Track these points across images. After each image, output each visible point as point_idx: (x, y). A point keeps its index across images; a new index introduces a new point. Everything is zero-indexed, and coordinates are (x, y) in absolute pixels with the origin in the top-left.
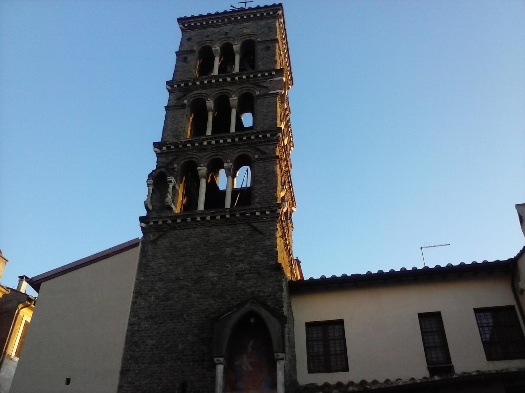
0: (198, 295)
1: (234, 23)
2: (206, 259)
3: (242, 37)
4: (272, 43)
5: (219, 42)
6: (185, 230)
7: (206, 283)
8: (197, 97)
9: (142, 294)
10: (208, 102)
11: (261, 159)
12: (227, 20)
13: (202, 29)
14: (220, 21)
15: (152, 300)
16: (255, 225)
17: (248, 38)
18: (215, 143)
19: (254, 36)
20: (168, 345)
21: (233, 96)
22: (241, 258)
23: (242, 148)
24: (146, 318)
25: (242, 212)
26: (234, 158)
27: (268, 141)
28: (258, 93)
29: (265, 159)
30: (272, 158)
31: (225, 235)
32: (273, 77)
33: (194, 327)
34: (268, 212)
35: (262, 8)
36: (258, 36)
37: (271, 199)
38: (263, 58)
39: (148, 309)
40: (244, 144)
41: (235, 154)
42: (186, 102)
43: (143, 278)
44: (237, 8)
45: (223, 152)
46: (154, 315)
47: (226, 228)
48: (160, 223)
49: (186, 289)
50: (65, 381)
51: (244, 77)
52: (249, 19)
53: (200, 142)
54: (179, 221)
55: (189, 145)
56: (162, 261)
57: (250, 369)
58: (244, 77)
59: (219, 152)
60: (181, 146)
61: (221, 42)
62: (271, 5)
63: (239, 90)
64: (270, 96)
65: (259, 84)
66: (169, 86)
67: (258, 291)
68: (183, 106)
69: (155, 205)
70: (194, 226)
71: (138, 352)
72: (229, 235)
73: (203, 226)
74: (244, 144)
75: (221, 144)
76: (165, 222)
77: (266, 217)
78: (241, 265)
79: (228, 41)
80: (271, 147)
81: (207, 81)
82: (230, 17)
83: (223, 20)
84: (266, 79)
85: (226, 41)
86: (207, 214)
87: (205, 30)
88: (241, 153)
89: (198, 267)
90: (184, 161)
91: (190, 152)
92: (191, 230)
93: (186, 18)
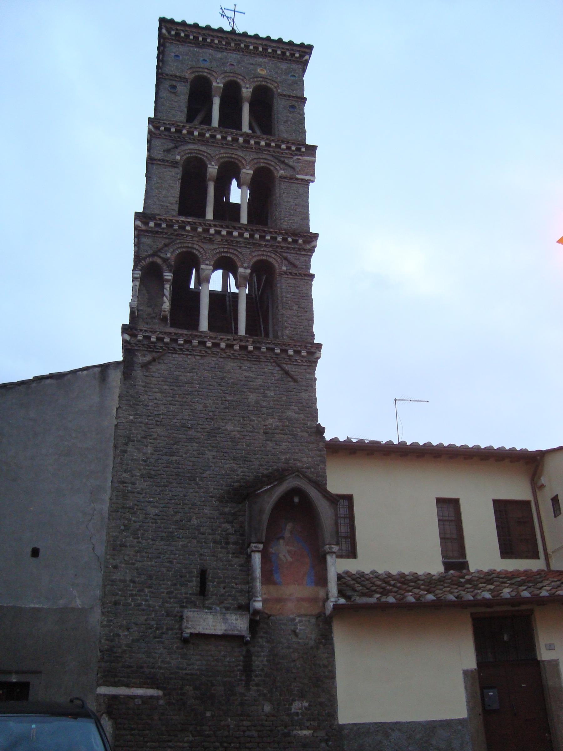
0: (214, 454)
1: (243, 52)
2: (222, 404)
3: (255, 79)
4: (297, 101)
5: (223, 76)
6: (190, 357)
7: (224, 438)
8: (194, 155)
9: (133, 441)
10: (211, 168)
11: (291, 273)
12: (234, 45)
13: (196, 47)
14: (224, 43)
15: (149, 451)
16: (287, 367)
17: (263, 83)
18: (191, 229)
19: (272, 83)
20: (178, 517)
21: (248, 168)
22: (270, 411)
23: (263, 251)
24: (142, 476)
25: (270, 346)
26: (251, 263)
27: (299, 249)
28: (282, 172)
29: (296, 274)
30: (305, 275)
31: (246, 374)
32: (302, 154)
33: (212, 497)
34: (304, 353)
35: (285, 43)
36: (278, 85)
37: (305, 334)
38: (286, 122)
39: (144, 463)
40: (266, 245)
41: (253, 257)
42: (178, 158)
43: (133, 417)
44: (227, 15)
45: (238, 251)
46: (153, 472)
47: (247, 364)
48: (153, 339)
49: (196, 443)
50: (29, 550)
51: (263, 143)
52: (264, 54)
53: (204, 227)
54: (181, 342)
55: (188, 228)
56: (159, 395)
57: (290, 559)
58: (263, 143)
59: (232, 249)
60: (176, 227)
61: (225, 76)
62: (299, 43)
63: (255, 161)
64: (299, 182)
65: (283, 159)
66: (152, 125)
67: (295, 460)
68: (174, 164)
69: (141, 310)
70: (202, 353)
71: (135, 522)
72: (251, 374)
73: (215, 356)
74: (266, 245)
75: (235, 237)
76: (160, 339)
77: (302, 359)
78: (270, 421)
79: (235, 79)
80: (302, 259)
81: (210, 134)
82: (239, 43)
83: (228, 43)
84: (293, 155)
85: (232, 79)
86: (222, 339)
87: (200, 50)
88: (262, 258)
89: (211, 414)
90: (179, 251)
91: (190, 238)
92: (197, 357)
93: (172, 21)
